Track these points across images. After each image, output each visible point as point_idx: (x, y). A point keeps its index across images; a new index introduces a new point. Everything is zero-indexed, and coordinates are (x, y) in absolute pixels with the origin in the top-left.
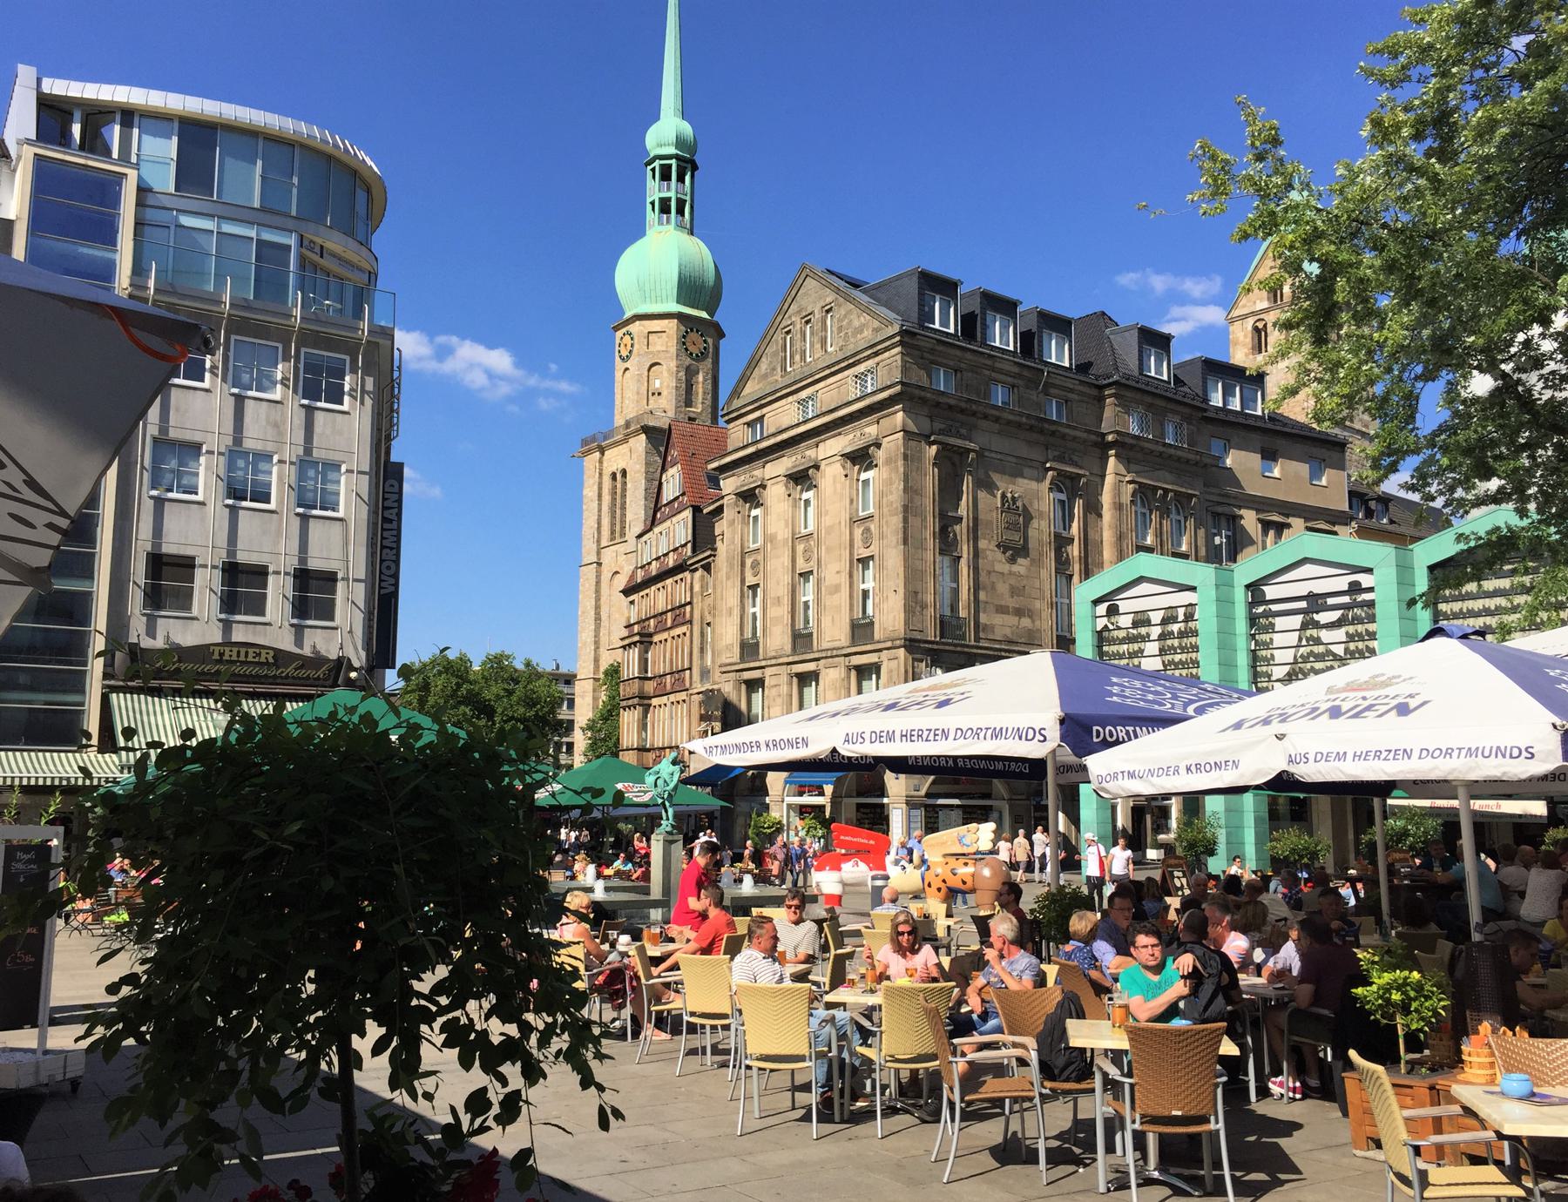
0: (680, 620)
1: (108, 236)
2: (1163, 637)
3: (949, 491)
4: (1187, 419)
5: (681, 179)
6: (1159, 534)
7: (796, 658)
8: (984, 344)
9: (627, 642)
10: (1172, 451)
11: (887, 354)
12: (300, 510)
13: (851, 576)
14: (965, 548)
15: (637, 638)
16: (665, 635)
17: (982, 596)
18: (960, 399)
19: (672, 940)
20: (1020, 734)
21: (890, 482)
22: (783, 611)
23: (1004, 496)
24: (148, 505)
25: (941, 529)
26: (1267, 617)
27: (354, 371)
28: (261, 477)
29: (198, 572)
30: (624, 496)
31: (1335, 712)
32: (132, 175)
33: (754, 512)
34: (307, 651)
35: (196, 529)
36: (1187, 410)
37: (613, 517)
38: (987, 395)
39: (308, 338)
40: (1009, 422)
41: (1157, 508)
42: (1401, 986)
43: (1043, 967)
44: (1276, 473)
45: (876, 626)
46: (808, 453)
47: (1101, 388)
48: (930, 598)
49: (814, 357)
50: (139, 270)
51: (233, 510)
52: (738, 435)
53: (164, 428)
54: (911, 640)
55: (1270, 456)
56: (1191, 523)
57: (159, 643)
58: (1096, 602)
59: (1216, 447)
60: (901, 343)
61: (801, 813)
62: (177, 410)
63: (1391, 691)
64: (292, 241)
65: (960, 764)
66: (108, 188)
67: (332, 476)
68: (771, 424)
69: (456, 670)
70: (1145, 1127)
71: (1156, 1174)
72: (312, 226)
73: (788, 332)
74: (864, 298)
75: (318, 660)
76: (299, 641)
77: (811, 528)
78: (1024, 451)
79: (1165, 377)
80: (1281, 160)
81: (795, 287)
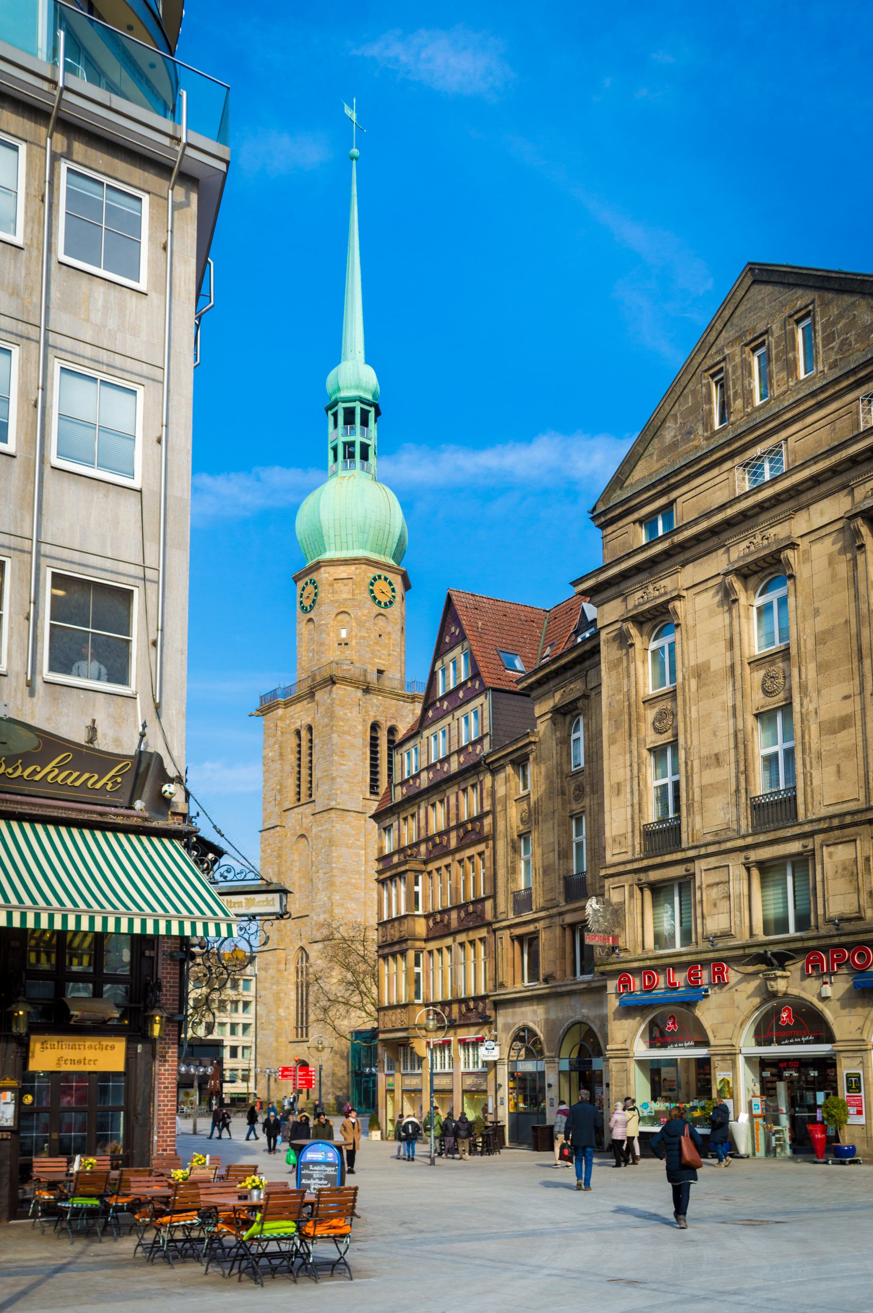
5: (365, 423)
7: (762, 838)
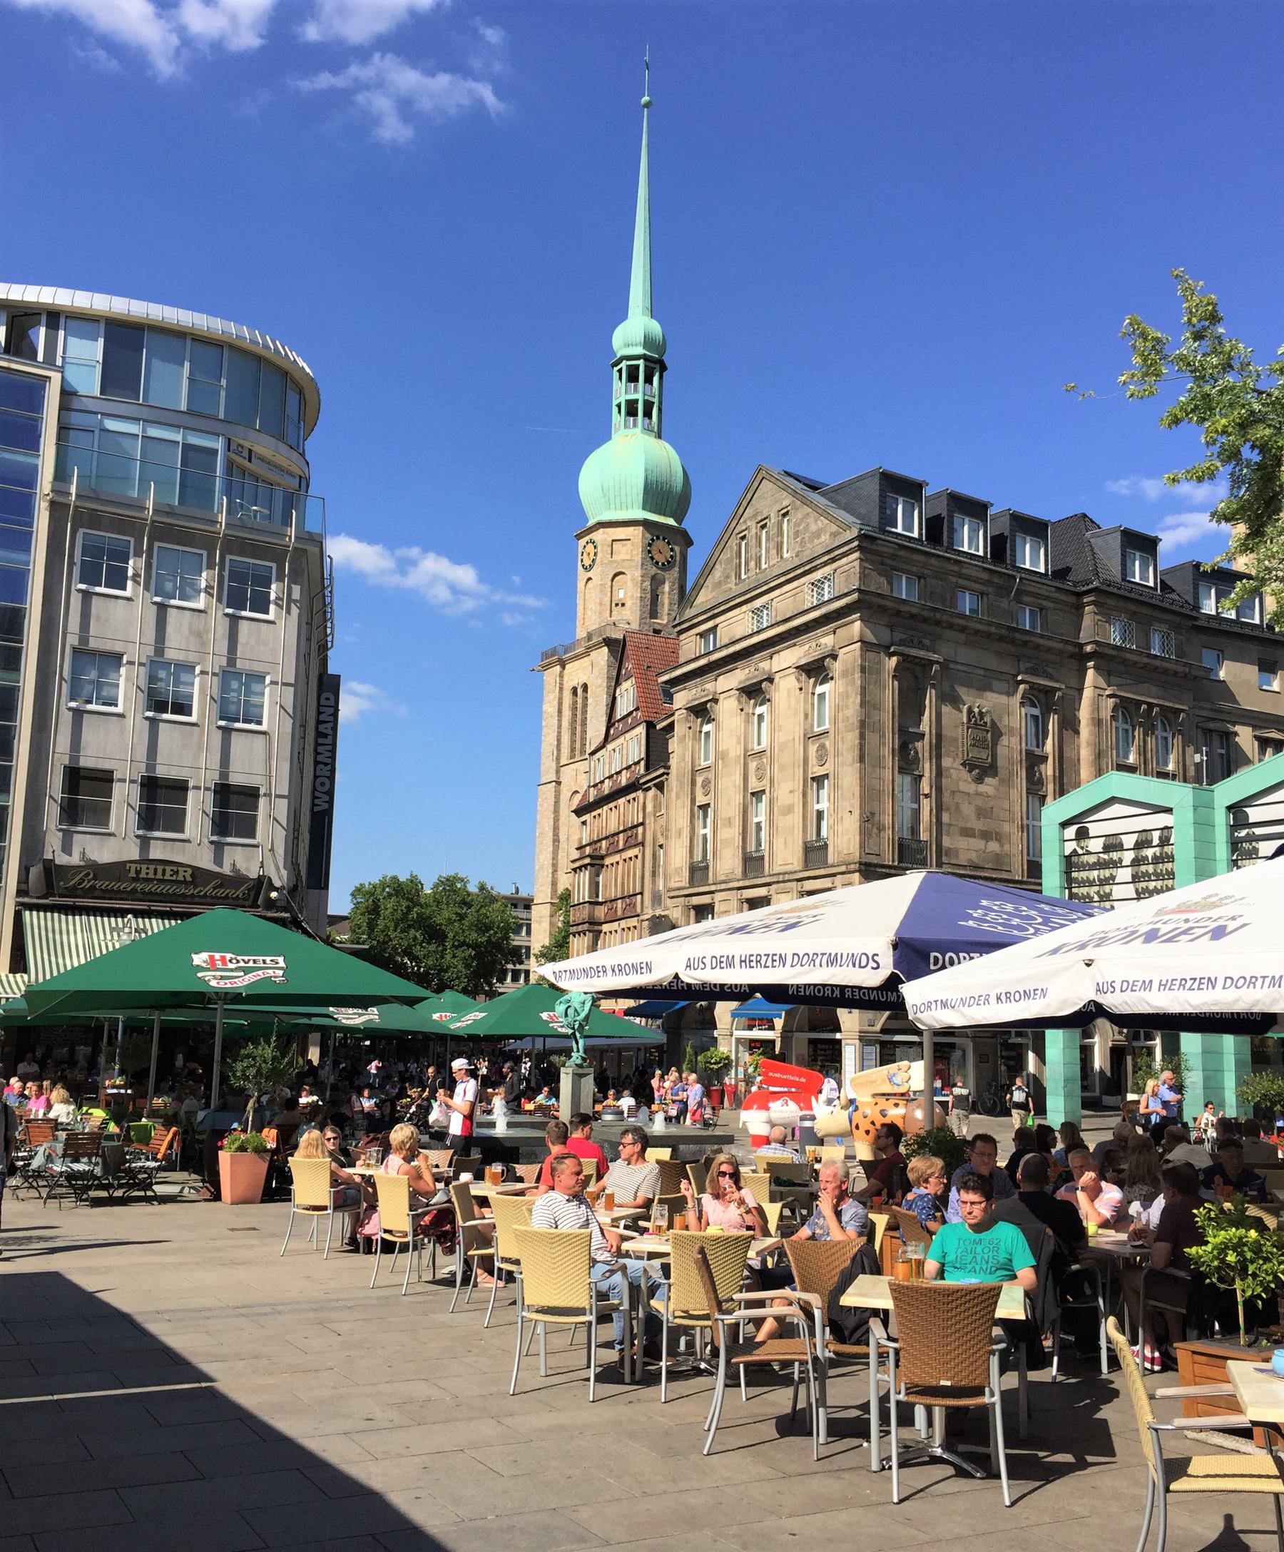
0: (632, 842)
1: (31, 442)
2: (1136, 862)
3: (910, 706)
4: (1177, 628)
5: (649, 380)
6: (1143, 752)
7: (747, 883)
8: (950, 548)
9: (577, 864)
10: (1158, 663)
11: (844, 560)
12: (222, 723)
13: (804, 795)
14: (927, 766)
15: (587, 861)
16: (616, 858)
17: (945, 817)
18: (923, 607)
19: (521, 1180)
20: (855, 961)
21: (845, 696)
22: (731, 834)
23: (970, 711)
24: (67, 717)
25: (902, 746)
26: (1250, 841)
27: (280, 579)
28: (182, 689)
29: (116, 787)
30: (584, 712)
31: (1151, 936)
32: (56, 377)
33: (706, 728)
34: (227, 869)
35: (115, 740)
36: (1177, 619)
37: (573, 734)
38: (953, 603)
39: (234, 545)
40: (977, 632)
41: (1141, 724)
42: (1238, 1246)
43: (871, 1216)
44: (1276, 686)
45: (830, 849)
46: (761, 665)
47: (1080, 595)
48: (887, 820)
49: (770, 564)
50: (61, 475)
51: (153, 722)
52: (690, 645)
53: (84, 639)
54: (868, 865)
55: (1268, 667)
56: (1178, 740)
57: (75, 860)
58: (1065, 825)
59: (1208, 658)
60: (860, 548)
61: (751, 1048)
62: (98, 619)
63: (1214, 913)
64: (219, 444)
65: (848, 994)
66: (32, 391)
67: (256, 687)
68: (724, 635)
69: (405, 891)
70: (912, 1399)
71: (939, 1452)
72: (240, 430)
73: (743, 538)
74: (822, 501)
75: (237, 879)
76: (218, 860)
77: (764, 744)
78: (993, 663)
79: (1151, 584)
80: (1219, 339)
81: (750, 492)
